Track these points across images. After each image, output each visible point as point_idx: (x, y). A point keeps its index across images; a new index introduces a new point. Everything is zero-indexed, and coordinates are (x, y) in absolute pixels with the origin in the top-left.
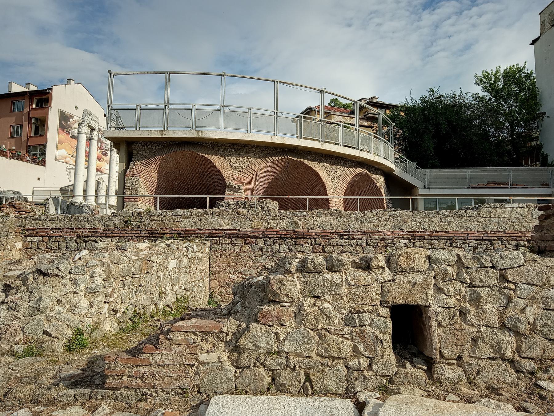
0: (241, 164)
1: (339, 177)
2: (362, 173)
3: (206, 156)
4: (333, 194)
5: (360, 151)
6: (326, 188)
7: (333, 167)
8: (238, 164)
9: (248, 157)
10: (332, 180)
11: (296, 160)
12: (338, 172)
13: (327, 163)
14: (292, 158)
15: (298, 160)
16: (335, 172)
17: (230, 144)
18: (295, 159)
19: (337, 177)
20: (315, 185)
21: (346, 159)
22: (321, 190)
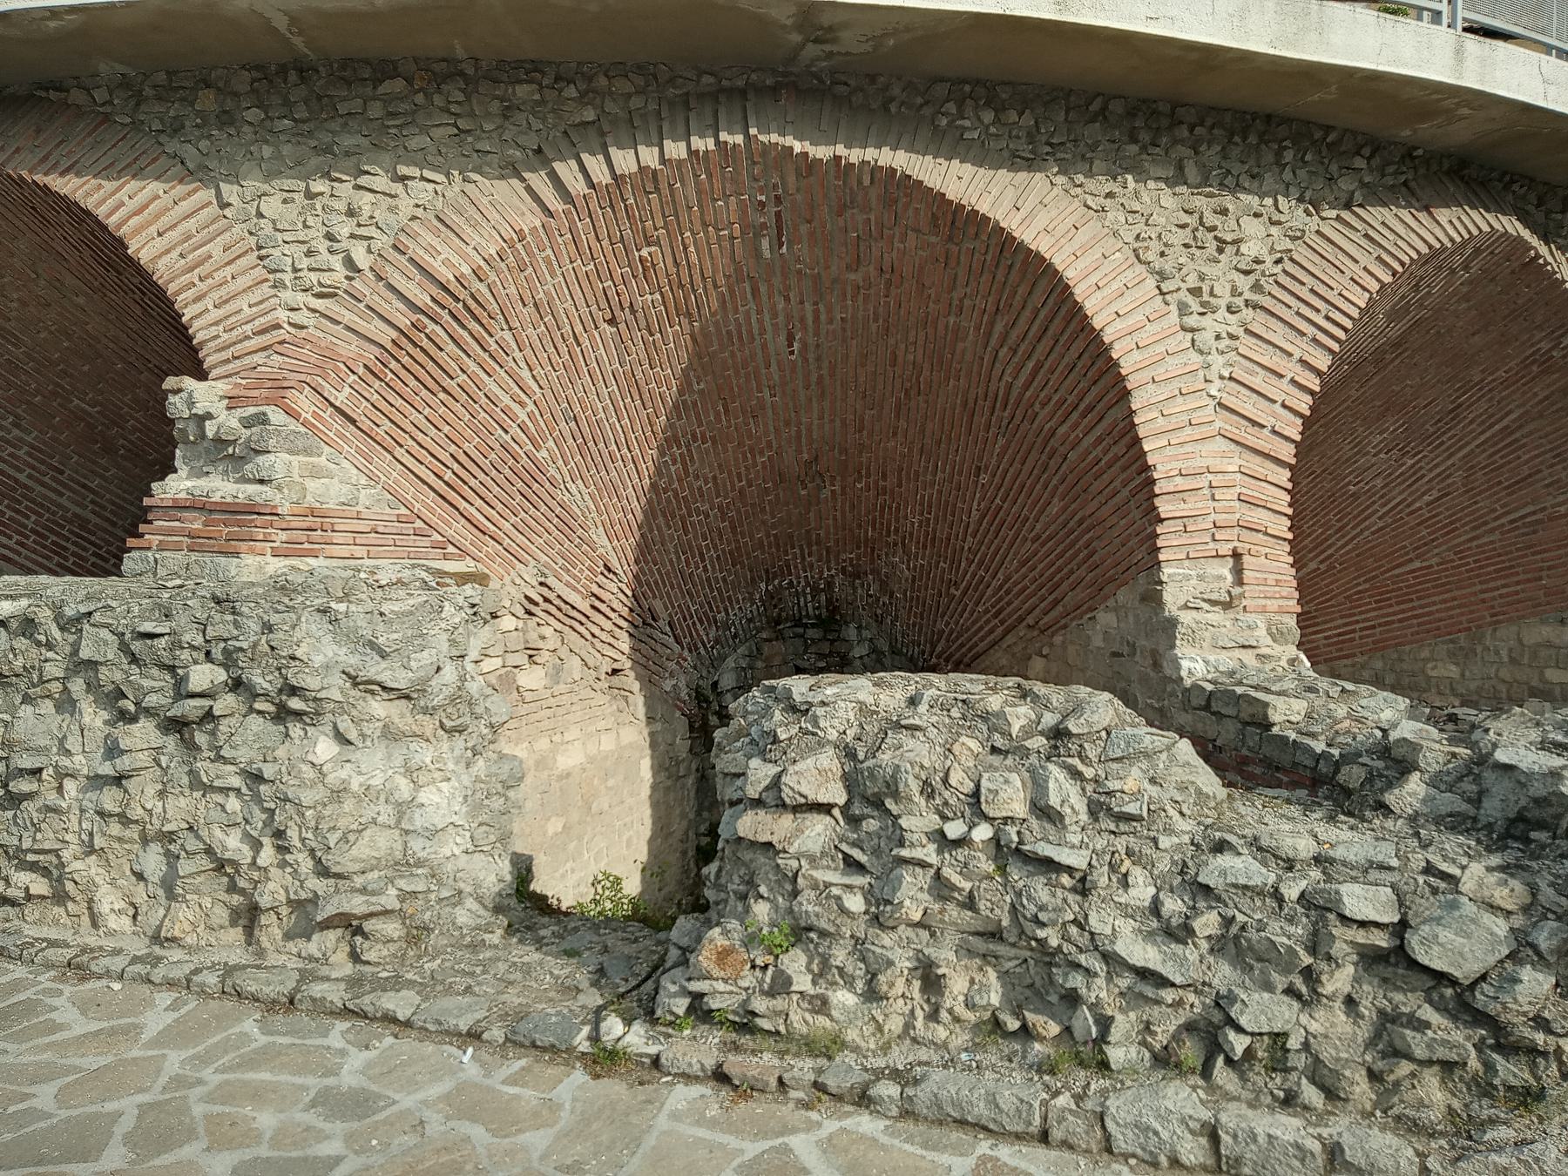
0: (344, 229)
1: (1257, 287)
2: (1476, 248)
3: (65, 185)
4: (1197, 433)
5: (1472, 42)
6: (1126, 394)
7: (1199, 202)
8: (316, 237)
9: (403, 170)
10: (1192, 321)
11: (837, 158)
12: (1250, 249)
13: (1142, 177)
14: (789, 141)
15: (855, 155)
16: (1221, 245)
17: (258, 68)
18: (822, 152)
19: (1235, 292)
20: (1039, 366)
21: (1328, 129)
22: (1090, 409)
